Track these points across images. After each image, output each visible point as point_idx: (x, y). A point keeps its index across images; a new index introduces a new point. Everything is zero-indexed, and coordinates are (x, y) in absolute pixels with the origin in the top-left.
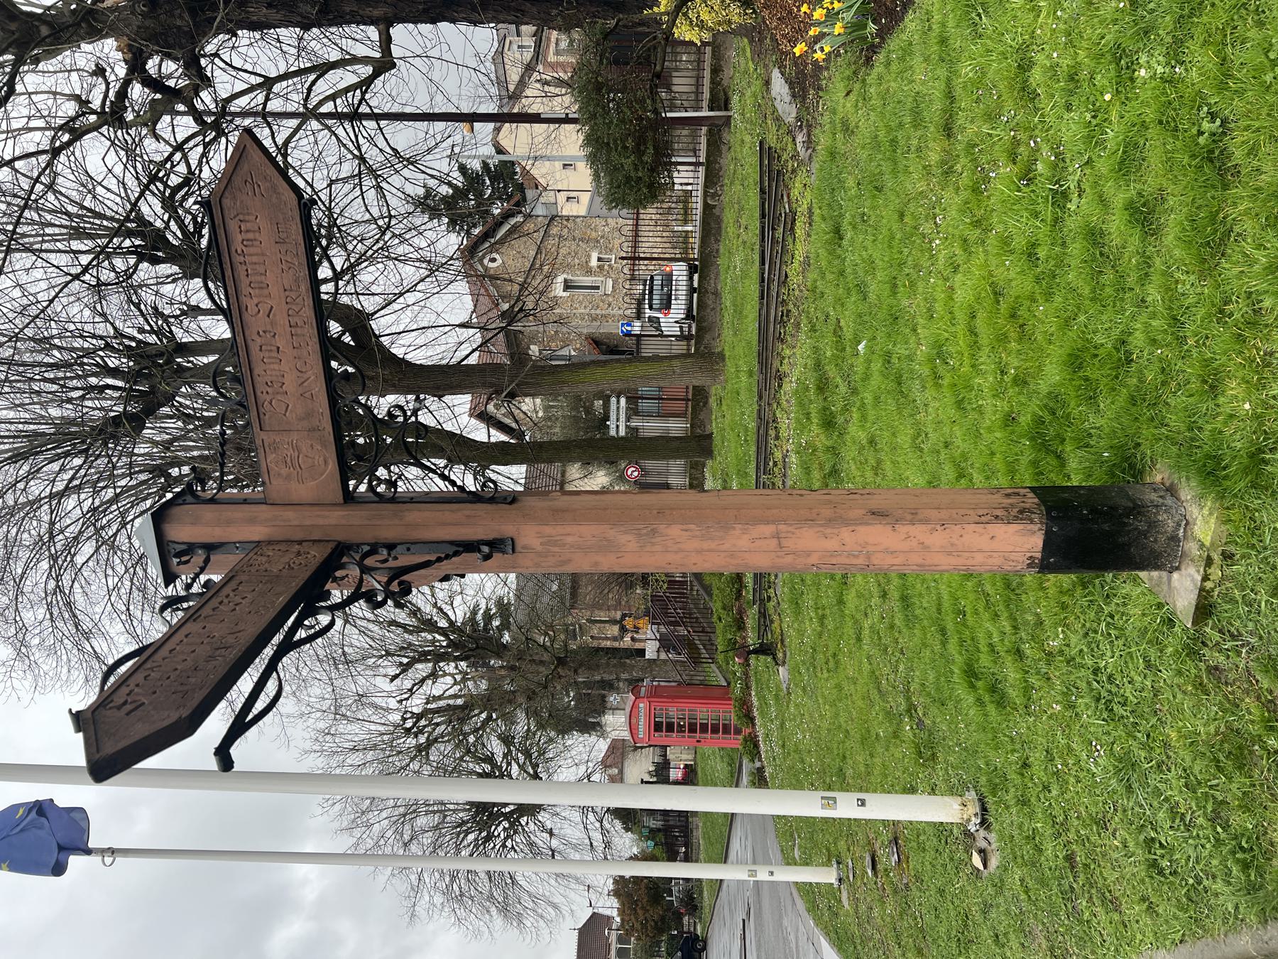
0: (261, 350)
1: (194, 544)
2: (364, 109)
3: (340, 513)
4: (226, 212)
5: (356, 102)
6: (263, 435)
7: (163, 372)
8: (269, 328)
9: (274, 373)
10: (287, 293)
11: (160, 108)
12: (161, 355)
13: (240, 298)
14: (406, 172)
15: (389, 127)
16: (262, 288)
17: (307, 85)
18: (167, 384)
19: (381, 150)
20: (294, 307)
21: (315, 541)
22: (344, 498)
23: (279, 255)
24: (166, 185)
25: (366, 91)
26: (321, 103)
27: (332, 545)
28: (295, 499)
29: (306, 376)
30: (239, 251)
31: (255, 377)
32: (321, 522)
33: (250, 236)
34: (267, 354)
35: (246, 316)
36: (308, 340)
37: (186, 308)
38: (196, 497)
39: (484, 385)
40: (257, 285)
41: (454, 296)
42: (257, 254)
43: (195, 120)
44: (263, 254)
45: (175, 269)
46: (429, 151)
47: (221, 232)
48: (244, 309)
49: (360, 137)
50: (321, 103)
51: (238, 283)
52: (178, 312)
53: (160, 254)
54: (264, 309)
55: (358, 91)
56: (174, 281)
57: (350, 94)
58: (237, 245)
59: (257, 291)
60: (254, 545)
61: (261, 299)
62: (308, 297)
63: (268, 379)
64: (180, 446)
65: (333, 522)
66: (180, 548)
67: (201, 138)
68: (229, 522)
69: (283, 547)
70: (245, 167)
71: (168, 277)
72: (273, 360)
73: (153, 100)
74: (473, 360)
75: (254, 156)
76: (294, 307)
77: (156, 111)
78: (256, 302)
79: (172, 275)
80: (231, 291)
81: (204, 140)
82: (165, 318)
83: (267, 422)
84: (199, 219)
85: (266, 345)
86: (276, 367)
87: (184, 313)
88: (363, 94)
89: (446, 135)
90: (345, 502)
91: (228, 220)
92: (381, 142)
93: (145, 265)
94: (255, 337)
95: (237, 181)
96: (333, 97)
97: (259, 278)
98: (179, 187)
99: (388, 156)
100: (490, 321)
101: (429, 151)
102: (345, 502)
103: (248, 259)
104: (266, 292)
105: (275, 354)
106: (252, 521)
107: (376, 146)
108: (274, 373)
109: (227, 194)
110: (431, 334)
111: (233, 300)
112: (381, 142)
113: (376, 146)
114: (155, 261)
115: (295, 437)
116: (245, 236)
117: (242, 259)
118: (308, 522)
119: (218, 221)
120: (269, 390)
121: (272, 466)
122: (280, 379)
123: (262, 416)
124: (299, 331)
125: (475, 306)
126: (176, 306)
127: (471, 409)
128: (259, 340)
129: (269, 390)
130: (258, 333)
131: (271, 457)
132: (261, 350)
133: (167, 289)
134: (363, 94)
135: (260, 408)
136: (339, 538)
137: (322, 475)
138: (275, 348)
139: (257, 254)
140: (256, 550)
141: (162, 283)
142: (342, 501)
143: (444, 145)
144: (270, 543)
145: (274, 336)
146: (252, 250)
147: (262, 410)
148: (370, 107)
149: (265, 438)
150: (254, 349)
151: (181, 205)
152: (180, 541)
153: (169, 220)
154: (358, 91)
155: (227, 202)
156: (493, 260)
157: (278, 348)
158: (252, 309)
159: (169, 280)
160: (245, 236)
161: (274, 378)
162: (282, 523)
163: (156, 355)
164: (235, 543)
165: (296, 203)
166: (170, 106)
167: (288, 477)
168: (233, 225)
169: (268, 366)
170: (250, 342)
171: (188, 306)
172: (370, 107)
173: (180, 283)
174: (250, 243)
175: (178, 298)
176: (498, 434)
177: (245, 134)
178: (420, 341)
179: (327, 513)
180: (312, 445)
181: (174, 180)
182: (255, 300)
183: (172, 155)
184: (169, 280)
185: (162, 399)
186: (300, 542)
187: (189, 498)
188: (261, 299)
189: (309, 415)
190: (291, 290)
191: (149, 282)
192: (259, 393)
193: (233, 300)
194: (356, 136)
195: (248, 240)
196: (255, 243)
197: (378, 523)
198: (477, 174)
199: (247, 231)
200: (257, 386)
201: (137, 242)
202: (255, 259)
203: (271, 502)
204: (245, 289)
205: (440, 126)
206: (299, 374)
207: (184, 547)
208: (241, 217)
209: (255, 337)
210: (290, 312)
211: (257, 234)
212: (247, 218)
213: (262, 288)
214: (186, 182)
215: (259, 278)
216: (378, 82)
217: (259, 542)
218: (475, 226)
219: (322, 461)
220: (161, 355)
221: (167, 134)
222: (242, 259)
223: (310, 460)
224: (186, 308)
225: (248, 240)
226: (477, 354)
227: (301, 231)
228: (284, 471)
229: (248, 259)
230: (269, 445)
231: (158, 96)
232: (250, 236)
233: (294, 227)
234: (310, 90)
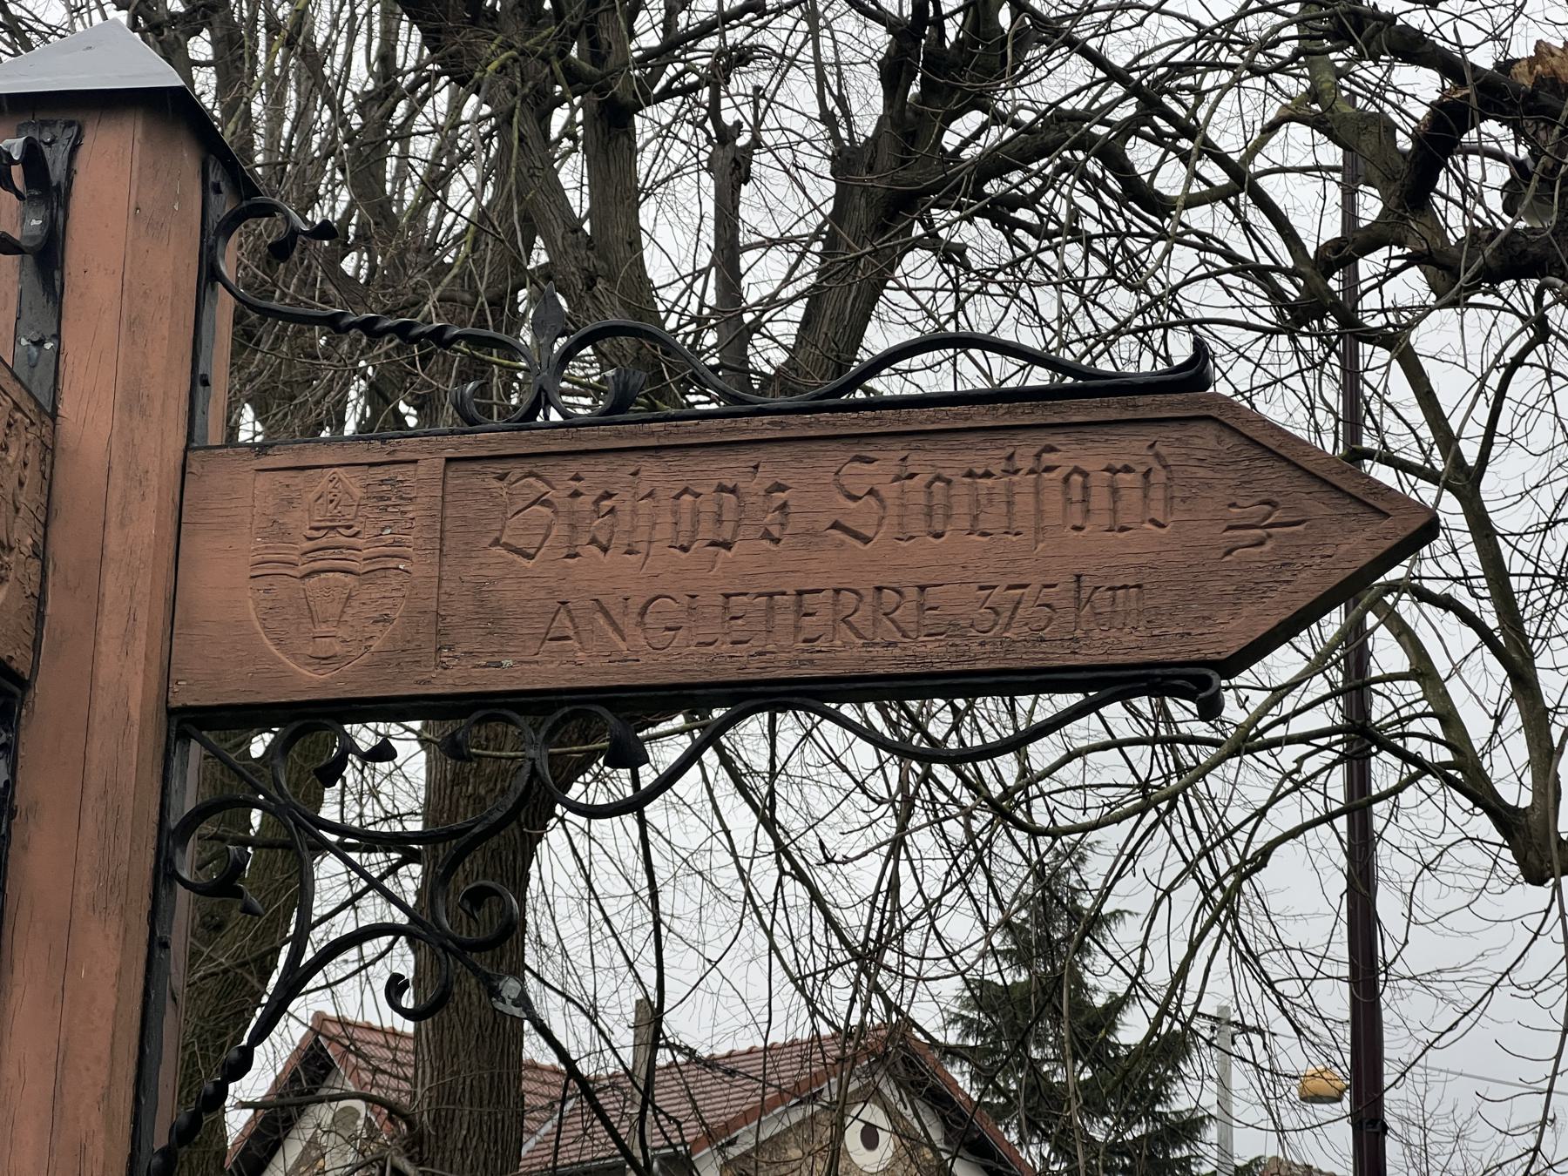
0: (722, 489)
1: (65, 206)
2: (1384, 770)
3: (136, 715)
4: (1172, 432)
5: (1413, 745)
6: (429, 465)
7: (545, 59)
8: (797, 523)
9: (643, 522)
10: (912, 593)
11: (1368, 144)
12: (597, 54)
13: (897, 444)
14: (1189, 893)
15: (1330, 844)
16: (929, 515)
17: (1461, 594)
18: (503, 67)
19: (1261, 813)
20: (866, 610)
21: (41, 600)
22: (186, 709)
23: (1036, 581)
24: (1129, 128)
25: (1450, 781)
26: (1405, 635)
27: (21, 665)
28: (197, 545)
29: (628, 623)
30: (1048, 458)
31: (631, 462)
32: (111, 627)
33: (1100, 499)
34: (708, 506)
35: (837, 455)
36: (756, 645)
37: (742, 141)
38: (228, 227)
39: (445, 1095)
40: (939, 498)
41: (759, 1006)
42: (1040, 512)
43: (1335, 245)
44: (1039, 530)
45: (866, 125)
46: (1250, 958)
47: (1112, 409)
48: (858, 450)
49: (1304, 749)
50: (1405, 635)
51: (945, 441)
52: (729, 117)
53: (914, 89)
54: (860, 514)
55: (1445, 755)
56: (827, 118)
57: (1434, 726)
58: (1068, 454)
59: (921, 498)
60: (45, 400)
61: (893, 510)
62: (899, 661)
63: (623, 501)
64: (394, 181)
65: (106, 673)
66: (55, 159)
67: (1288, 261)
68: (133, 325)
69: (29, 498)
70: (1317, 506)
71: (841, 101)
72: (685, 526)
73: (1392, 127)
74: (534, 1049)
75: (1357, 540)
76: (866, 610)
77: (1360, 132)
78: (884, 491)
79: (847, 114)
80: (921, 419)
81: (1278, 268)
82: (717, 78)
83: (476, 481)
84: (1023, 214)
85: (741, 507)
86: (664, 532)
87: (725, 135)
88: (1439, 770)
89: (1302, 1017)
90: (171, 712)
91: (1152, 433)
92: (1287, 814)
93: (879, 37)
94: (766, 477)
95: (1274, 479)
96: (1422, 670)
97: (961, 507)
98: (1122, 168)
99: (1241, 837)
100: (670, 1129)
101: (1250, 958)
102: (171, 712)
103: (1024, 482)
104: (917, 525)
105: (707, 531)
106: (133, 402)
107: (1274, 799)
108: (643, 522)
109: (1230, 441)
110: (632, 918)
111: (890, 421)
112: (1287, 814)
113: (1274, 799)
114: (893, 73)
115: (421, 568)
116: (1099, 480)
117: (1025, 463)
118: (112, 585)
119: (1147, 405)
120: (586, 501)
121: (322, 481)
122: (620, 541)
123: (499, 468)
124: (785, 619)
125: (711, 1063)
126: (747, 111)
127: (342, 1022)
128: (754, 486)
129: (586, 501)
130: (781, 488)
131: (353, 483)
132: (722, 489)
133: (800, 91)
134: (1439, 770)
135: (528, 466)
136: (39, 685)
137: (279, 643)
138: (727, 535)
139: (1040, 512)
140: (28, 406)
141: (821, 80)
142: (175, 703)
143: (1273, 1012)
144: (49, 450)
145: (767, 535)
146: (1053, 501)
147: (517, 469)
148: (1396, 791)
149: (422, 469)
150: (729, 468)
151: (1065, 167)
152: (80, 164)
153: (1016, 124)
154: (1445, 755)
155: (1206, 439)
156: (870, 1137)
157: (727, 546)
158: (860, 476)
159: (830, 103)
160: (1099, 480)
161: (625, 520)
162: (115, 497)
163: (595, 44)
164: (57, 336)
165: (1210, 653)
166: (1375, 175)
167: (277, 530)
168: (1132, 447)
169: (667, 504)
170: (748, 457)
171: (748, 150)
172: (1396, 791)
173: (817, 130)
174: (1076, 494)
175: (770, 121)
176: (240, 1126)
177: (1417, 523)
178: (607, 881)
179: (139, 648)
180: (386, 619)
181: (1142, 154)
182: (889, 491)
183: (1221, 159)
184: (830, 103)
185: (454, 44)
186: (41, 552)
187: (224, 205)
188: (893, 510)
189: (492, 619)
190: (921, 607)
191: (826, 43)
192: (574, 466)
193: (890, 421)
194: (1304, 738)
195: (1085, 488)
196: (1077, 508)
197: (89, 825)
198: (1157, 1097)
199: (1114, 491)
200: (603, 465)
201: (951, 31)
202: (1024, 502)
203: (194, 466)
204: (926, 461)
205: (1336, 1000)
206: (636, 604)
207: (57, 173)
208: (1159, 476)
209: (766, 477)
210: (846, 597)
211: (1106, 521)
212: (1157, 494)
213: (929, 515)
214: (1139, 193)
215: (961, 507)
216: (1483, 825)
217: (54, 415)
218: (983, 1076)
219: (323, 647)
220: (597, 54)
221: (1274, 151)
222: (1025, 463)
223: (335, 609)
224: (742, 141)
225: (1085, 488)
226: (550, 1059)
227: (1118, 659)
228: (299, 521)
229: (1024, 482)
230: (393, 482)
231: (1404, 143)
232: (1100, 499)
233: (1129, 640)
234: (1446, 603)
